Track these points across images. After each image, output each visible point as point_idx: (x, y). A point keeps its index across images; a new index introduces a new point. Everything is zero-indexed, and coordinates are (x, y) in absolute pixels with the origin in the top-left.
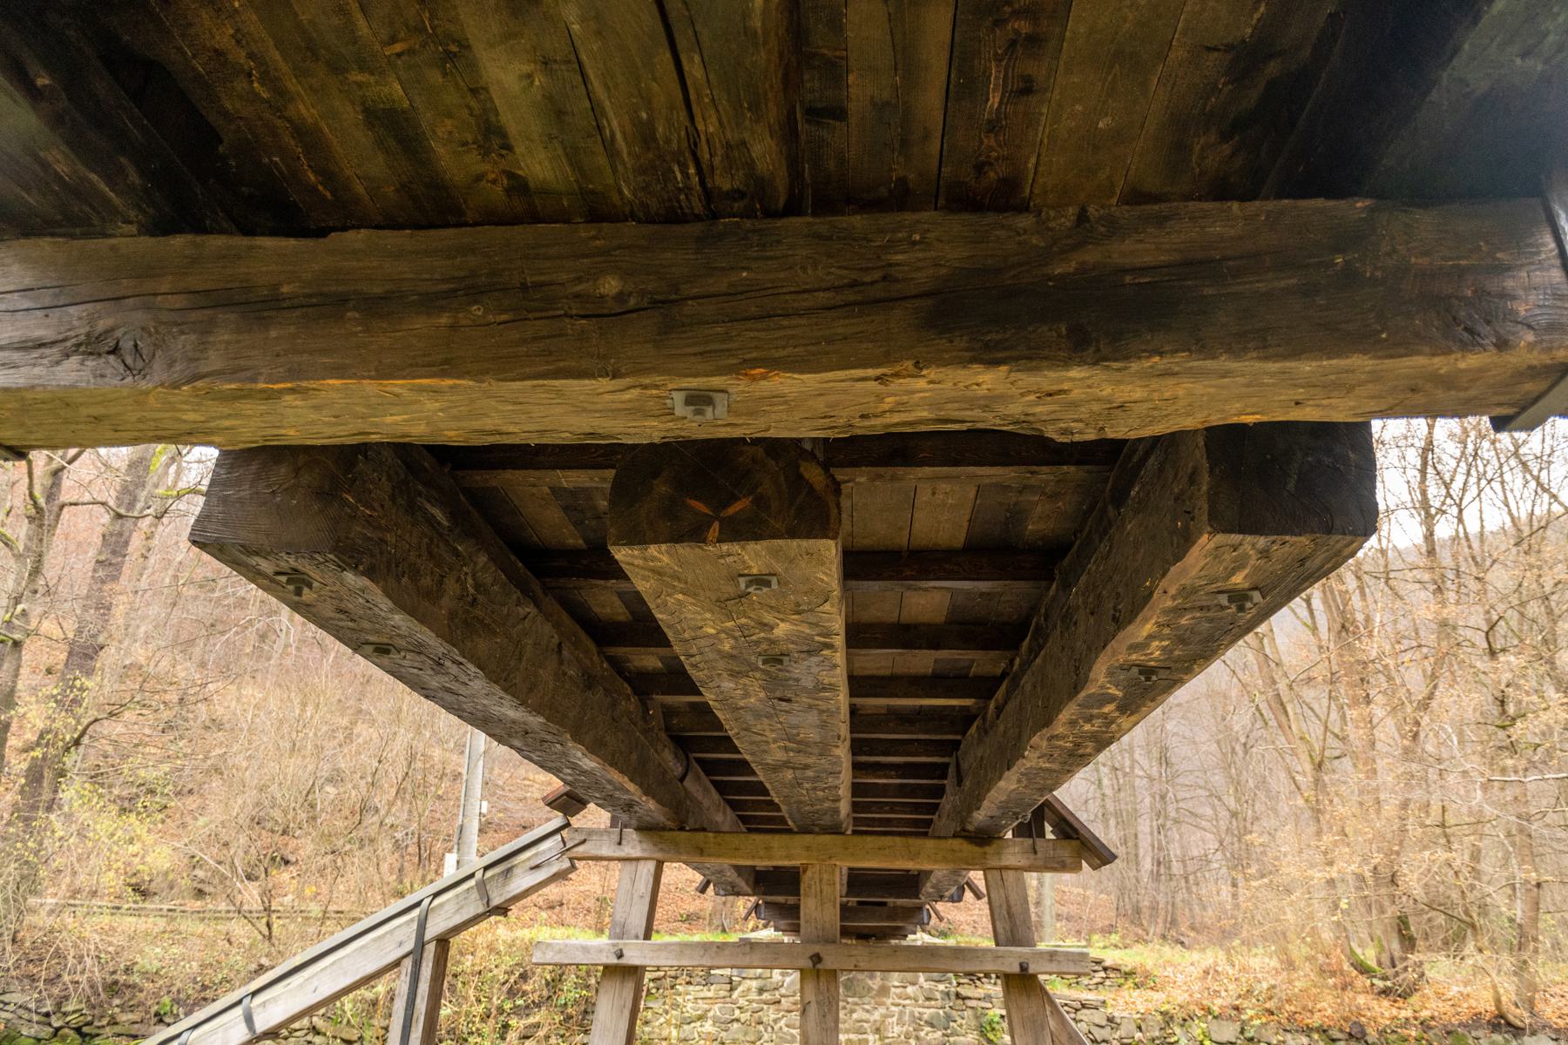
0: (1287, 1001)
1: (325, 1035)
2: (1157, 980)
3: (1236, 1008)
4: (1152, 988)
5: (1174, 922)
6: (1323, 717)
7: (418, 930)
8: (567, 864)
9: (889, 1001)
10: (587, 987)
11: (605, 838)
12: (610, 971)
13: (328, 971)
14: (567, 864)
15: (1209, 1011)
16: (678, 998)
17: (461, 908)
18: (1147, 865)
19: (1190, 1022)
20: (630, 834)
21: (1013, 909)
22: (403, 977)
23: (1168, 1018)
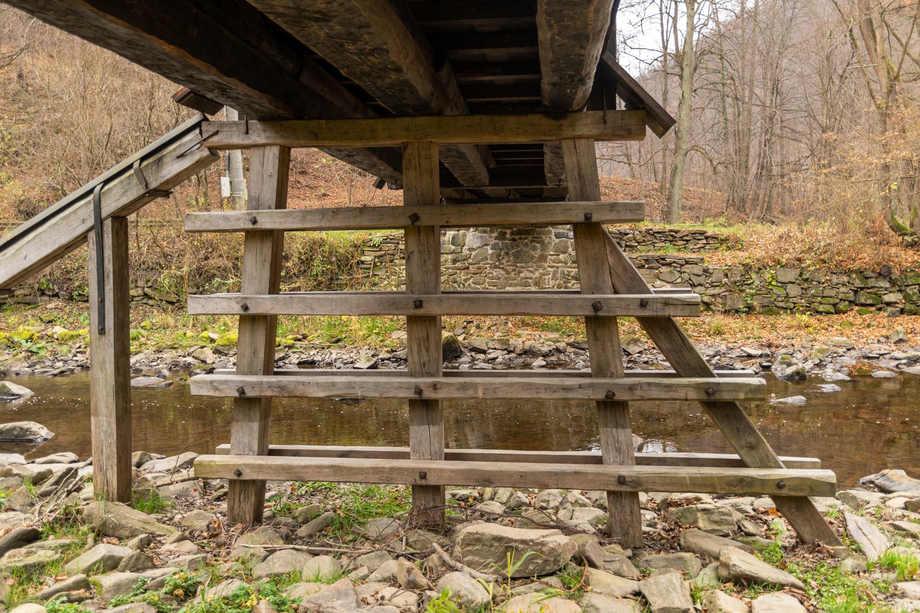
0: (837, 254)
1: (154, 299)
2: (744, 244)
3: (799, 260)
4: (739, 250)
5: (769, 209)
6: (904, 41)
7: (95, 210)
8: (206, 153)
9: (546, 265)
10: (331, 263)
11: (234, 129)
13: (32, 243)
14: (206, 153)
15: (779, 262)
16: (396, 268)
17: (126, 191)
18: (754, 170)
19: (764, 270)
20: (255, 124)
21: (584, 172)
22: (91, 246)
23: (747, 268)
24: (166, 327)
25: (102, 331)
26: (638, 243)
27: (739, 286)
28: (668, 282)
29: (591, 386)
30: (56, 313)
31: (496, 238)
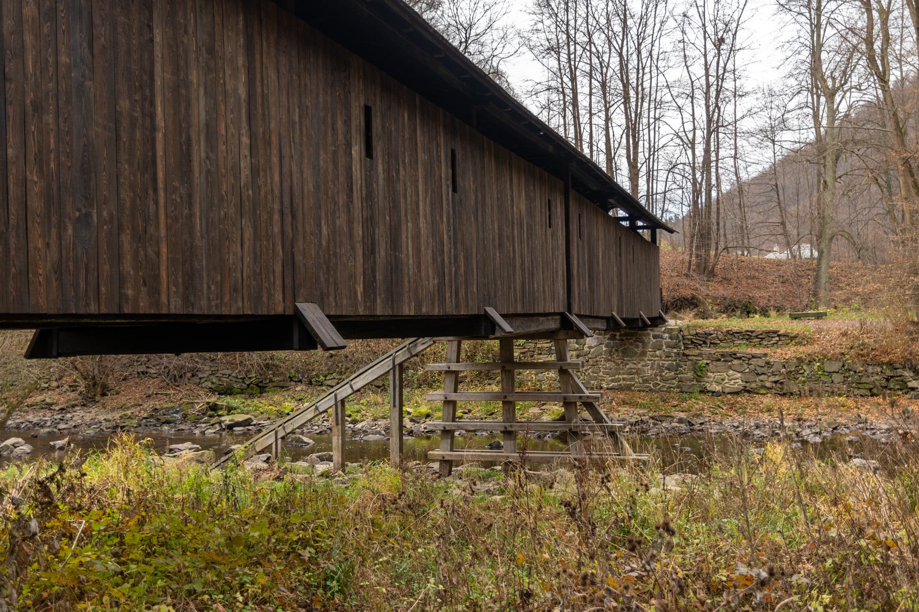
9: (646, 359)
10: (488, 358)
12: (447, 372)
23: (800, 360)
24: (376, 404)
25: (394, 406)
26: (721, 341)
27: (792, 375)
28: (738, 372)
29: (564, 426)
30: (303, 394)
31: (609, 339)
